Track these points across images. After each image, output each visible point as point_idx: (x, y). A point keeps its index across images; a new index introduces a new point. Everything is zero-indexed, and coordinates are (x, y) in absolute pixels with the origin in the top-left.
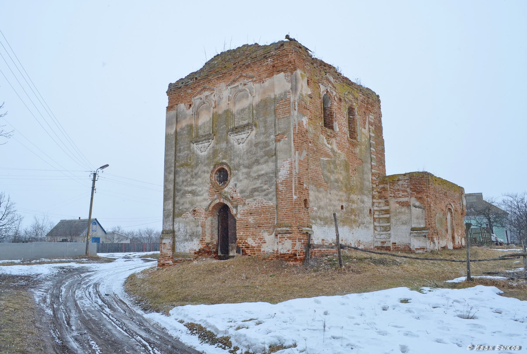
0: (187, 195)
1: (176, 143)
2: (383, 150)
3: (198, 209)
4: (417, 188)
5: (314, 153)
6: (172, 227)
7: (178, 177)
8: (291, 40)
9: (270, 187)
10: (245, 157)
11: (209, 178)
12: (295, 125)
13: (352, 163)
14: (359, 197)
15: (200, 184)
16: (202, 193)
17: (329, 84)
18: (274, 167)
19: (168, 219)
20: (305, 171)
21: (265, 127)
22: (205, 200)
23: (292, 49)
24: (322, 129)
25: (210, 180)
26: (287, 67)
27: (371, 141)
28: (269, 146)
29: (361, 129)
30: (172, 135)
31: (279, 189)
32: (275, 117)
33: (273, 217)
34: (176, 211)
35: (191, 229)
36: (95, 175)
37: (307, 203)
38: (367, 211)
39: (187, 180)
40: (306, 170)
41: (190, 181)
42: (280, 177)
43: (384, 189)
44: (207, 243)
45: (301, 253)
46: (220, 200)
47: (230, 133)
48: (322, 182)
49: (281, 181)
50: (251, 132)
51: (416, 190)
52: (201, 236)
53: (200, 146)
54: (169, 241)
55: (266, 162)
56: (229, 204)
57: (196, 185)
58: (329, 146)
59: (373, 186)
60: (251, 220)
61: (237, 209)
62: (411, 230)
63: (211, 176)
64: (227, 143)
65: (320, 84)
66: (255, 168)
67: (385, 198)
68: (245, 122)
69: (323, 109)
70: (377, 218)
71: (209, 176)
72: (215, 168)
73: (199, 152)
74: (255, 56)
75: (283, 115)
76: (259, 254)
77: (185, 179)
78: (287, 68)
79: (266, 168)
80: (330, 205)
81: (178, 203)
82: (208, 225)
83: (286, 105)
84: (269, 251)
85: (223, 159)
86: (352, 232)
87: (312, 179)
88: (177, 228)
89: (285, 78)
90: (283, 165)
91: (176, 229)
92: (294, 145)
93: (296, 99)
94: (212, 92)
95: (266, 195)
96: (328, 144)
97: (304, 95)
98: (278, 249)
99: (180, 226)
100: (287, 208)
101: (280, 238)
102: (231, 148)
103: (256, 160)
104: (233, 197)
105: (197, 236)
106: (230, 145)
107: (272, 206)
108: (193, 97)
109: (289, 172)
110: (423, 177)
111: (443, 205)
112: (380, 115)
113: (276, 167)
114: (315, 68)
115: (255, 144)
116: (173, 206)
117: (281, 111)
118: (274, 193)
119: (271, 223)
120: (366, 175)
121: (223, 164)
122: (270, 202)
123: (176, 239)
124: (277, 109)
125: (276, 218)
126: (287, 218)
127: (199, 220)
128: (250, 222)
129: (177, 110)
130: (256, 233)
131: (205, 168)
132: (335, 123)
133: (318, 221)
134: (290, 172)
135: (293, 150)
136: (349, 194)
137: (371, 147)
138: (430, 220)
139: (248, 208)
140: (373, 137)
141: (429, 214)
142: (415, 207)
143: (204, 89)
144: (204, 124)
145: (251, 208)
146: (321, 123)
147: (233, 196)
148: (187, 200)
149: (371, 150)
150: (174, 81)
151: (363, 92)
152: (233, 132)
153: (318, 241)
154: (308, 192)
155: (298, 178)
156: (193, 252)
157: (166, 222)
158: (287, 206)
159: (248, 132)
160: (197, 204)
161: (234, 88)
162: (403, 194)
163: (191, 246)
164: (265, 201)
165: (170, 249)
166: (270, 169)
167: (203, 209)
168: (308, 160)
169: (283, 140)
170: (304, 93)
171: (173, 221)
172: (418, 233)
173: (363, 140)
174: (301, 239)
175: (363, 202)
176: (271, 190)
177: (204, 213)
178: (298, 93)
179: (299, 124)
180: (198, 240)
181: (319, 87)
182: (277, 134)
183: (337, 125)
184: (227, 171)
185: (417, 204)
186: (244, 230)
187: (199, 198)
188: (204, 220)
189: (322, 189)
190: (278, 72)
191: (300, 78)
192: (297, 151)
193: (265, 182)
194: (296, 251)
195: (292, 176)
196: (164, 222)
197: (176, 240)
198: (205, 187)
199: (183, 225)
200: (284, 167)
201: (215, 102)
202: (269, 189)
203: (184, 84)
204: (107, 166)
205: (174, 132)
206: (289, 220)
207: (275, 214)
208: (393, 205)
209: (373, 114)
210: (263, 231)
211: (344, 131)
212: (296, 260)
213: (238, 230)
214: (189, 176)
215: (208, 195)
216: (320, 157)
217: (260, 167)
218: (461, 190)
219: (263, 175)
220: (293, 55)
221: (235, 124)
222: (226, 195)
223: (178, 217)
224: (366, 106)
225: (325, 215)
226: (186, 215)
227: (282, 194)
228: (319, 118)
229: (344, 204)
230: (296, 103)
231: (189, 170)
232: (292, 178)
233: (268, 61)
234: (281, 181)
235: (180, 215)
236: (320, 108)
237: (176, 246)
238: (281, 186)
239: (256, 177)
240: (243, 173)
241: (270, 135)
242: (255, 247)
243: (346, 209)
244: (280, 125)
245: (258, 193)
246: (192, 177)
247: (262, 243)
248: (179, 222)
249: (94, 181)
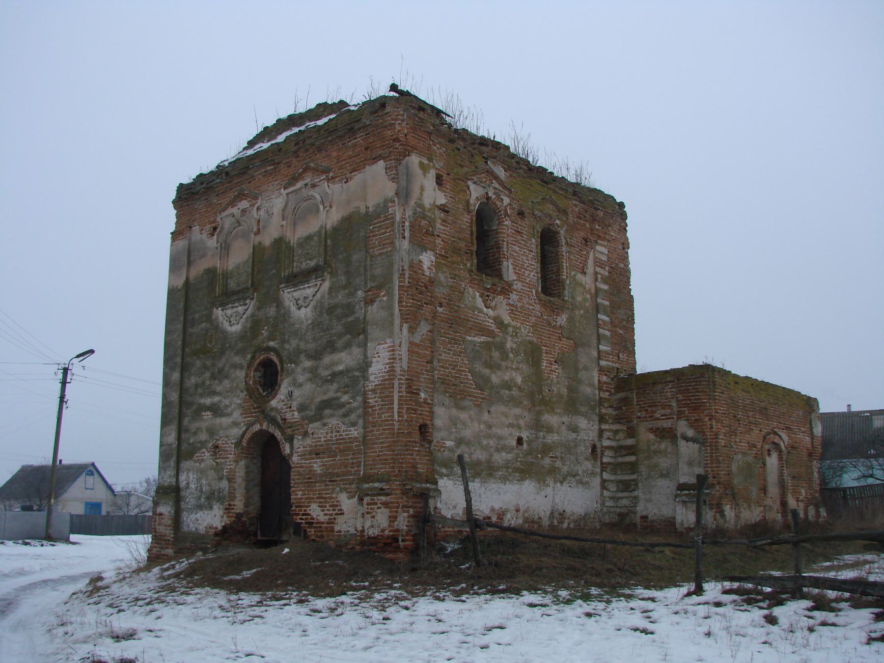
0: (204, 413)
1: (186, 308)
2: (631, 319)
3: (223, 444)
4: (690, 400)
5: (451, 327)
6: (175, 480)
8: (401, 93)
9: (353, 398)
10: (309, 336)
11: (244, 380)
12: (403, 270)
13: (548, 347)
14: (565, 419)
15: (228, 392)
16: (229, 410)
17: (494, 181)
18: (362, 357)
19: (168, 464)
20: (424, 365)
21: (347, 273)
22: (235, 424)
23: (401, 112)
24: (470, 275)
25: (244, 383)
26: (391, 149)
27: (599, 300)
28: (353, 312)
29: (575, 275)
30: (179, 290)
31: (369, 403)
32: (367, 252)
33: (357, 462)
34: (183, 448)
35: (209, 485)
36: (66, 371)
37: (427, 432)
38: (584, 450)
39: (204, 383)
40: (427, 362)
41: (210, 385)
42: (372, 378)
43: (626, 401)
44: (237, 514)
45: (407, 535)
46: (261, 425)
47: (282, 286)
48: (468, 387)
49: (373, 387)
50: (321, 284)
51: (688, 404)
52: (227, 498)
53: (229, 312)
54: (169, 509)
55: (347, 346)
56: (278, 434)
57: (219, 394)
58: (491, 312)
59: (602, 395)
60: (317, 466)
62: (678, 490)
63: (247, 376)
64: (277, 307)
65: (469, 183)
66: (327, 359)
67: (628, 422)
68: (312, 264)
69: (475, 234)
70: (609, 464)
71: (244, 375)
72: (253, 358)
73: (226, 325)
74: (335, 128)
75: (380, 249)
76: (331, 538)
77: (200, 380)
78: (391, 152)
79: (345, 359)
80: (490, 437)
81: (187, 430)
82: (239, 477)
83: (387, 228)
84: (348, 531)
85: (269, 339)
86: (543, 493)
87: (442, 383)
88: (184, 483)
89: (386, 173)
90: (378, 353)
91: (183, 484)
92: (400, 310)
93: (407, 216)
94: (254, 202)
95: (345, 415)
96: (487, 307)
97: (427, 206)
98: (363, 527)
99: (189, 478)
100: (381, 443)
101: (368, 504)
102: (284, 316)
103: (330, 341)
104: (285, 419)
105: (220, 500)
106: (282, 310)
107: (355, 438)
108: (220, 213)
109: (388, 366)
110: (702, 375)
111: (755, 436)
112: (626, 245)
113: (365, 356)
114: (459, 150)
115: (329, 309)
116: (177, 436)
117: (376, 240)
118: (360, 410)
119: (353, 472)
120: (584, 372)
121: (269, 349)
122: (352, 429)
123: (183, 505)
124: (371, 236)
125: (362, 463)
126: (381, 464)
127: (223, 466)
128: (315, 470)
130: (325, 494)
131: (237, 359)
132: (505, 263)
133: (455, 469)
134: (389, 367)
135: (397, 321)
136: (540, 413)
137: (598, 312)
138: (717, 467)
139: (313, 442)
140: (605, 291)
141: (714, 455)
142: (687, 439)
143: (241, 196)
144: (238, 267)
145: (318, 441)
146: (468, 265)
147: (287, 417)
148: (204, 425)
149: (598, 319)
150: (186, 181)
151: (580, 198)
152: (288, 285)
153: (453, 511)
154: (431, 408)
155: (406, 379)
156: (212, 532)
157: (165, 470)
158: (383, 438)
159: (316, 285)
160: (221, 433)
161: (294, 194)
162: (663, 412)
163: (210, 520)
164: (343, 428)
165: (169, 526)
166: (354, 360)
167: (232, 443)
168: (433, 342)
169: (380, 301)
170: (427, 202)
172: (690, 494)
173: (579, 298)
174: (409, 507)
175: (575, 429)
176: (355, 404)
177: (233, 452)
178: (412, 203)
179: (411, 266)
180: (221, 507)
181: (468, 188)
182: (369, 286)
183: (511, 267)
184: (276, 364)
185: (690, 433)
186: (305, 487)
187: (225, 421)
188: (233, 467)
189: (467, 403)
190: (374, 159)
191: (419, 171)
192: (406, 323)
194: (398, 530)
195: (393, 375)
196: (162, 469)
198: (235, 399)
199: (195, 476)
200: (379, 357)
201: (259, 221)
202: (351, 403)
203: (204, 185)
204: (92, 352)
205: (184, 284)
206: (386, 468)
207: (360, 454)
208: (645, 436)
209: (605, 243)
210: (338, 489)
211: (528, 280)
212: (398, 549)
213: (294, 487)
214: (207, 375)
215: (242, 414)
216: (465, 334)
217: (336, 357)
218: (810, 404)
219: (341, 373)
220: (404, 124)
221: (293, 267)
222: (273, 414)
223: (186, 460)
224: (588, 225)
225: (474, 457)
226: (201, 456)
227: (375, 414)
228: (466, 253)
229: (524, 435)
230: (407, 224)
231: (209, 363)
232: (394, 379)
233: (357, 138)
234: (373, 387)
235: (190, 455)
236: (469, 233)
238: (373, 396)
239: (329, 377)
240: (304, 369)
241: (356, 290)
242: (323, 523)
243: (529, 444)
244: (373, 270)
245: (332, 411)
246: (213, 377)
247: (336, 514)
248: (189, 470)
249: (64, 383)
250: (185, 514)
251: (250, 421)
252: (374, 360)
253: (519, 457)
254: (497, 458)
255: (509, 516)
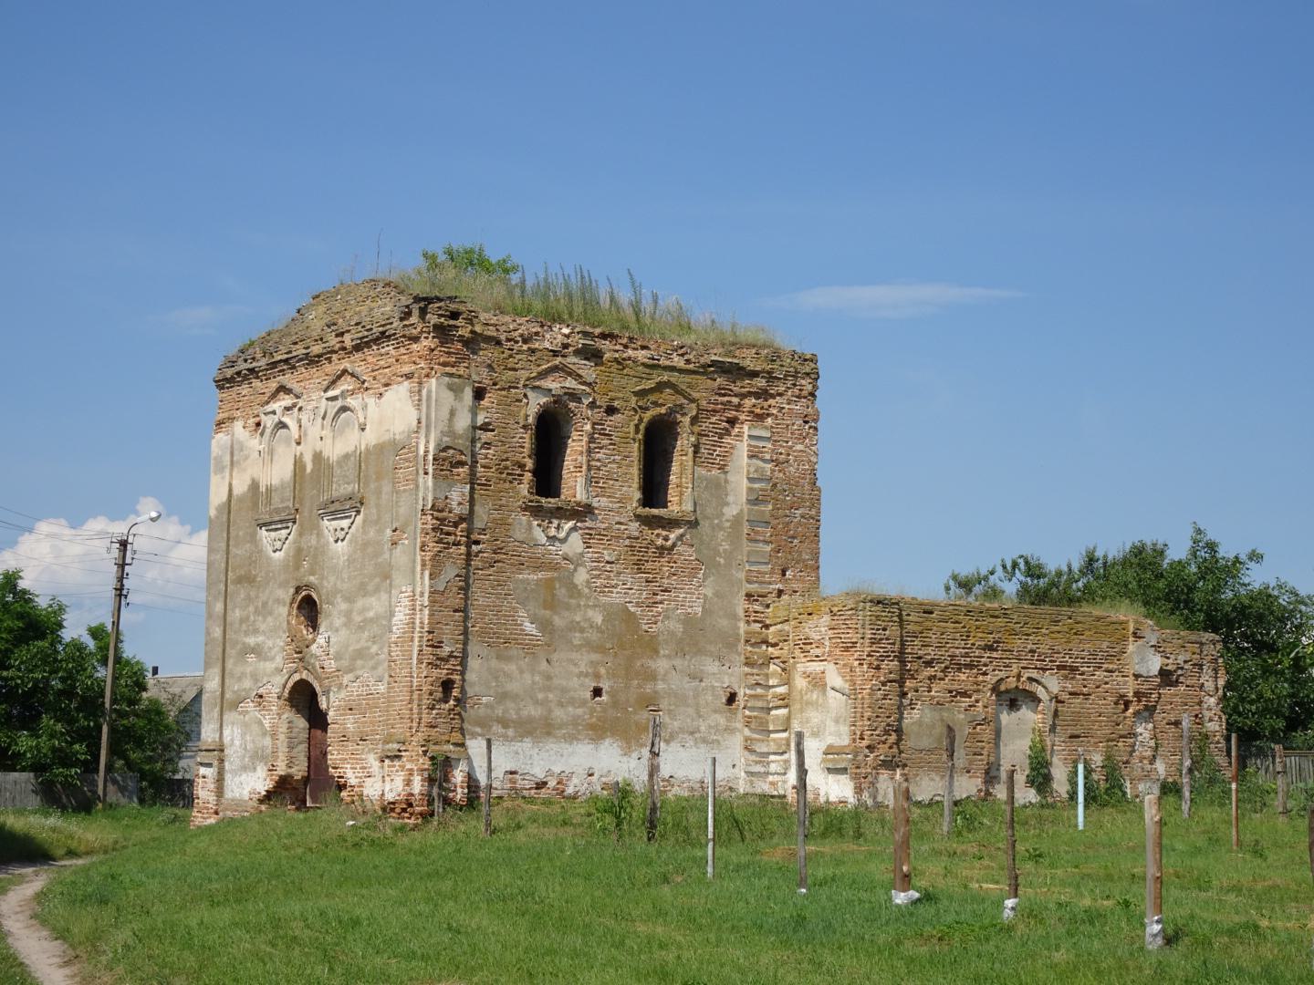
7: (233, 611)
16: (273, 653)
36: (124, 544)
55: (377, 590)
61: (328, 699)
66: (360, 603)
80: (548, 689)
88: (229, 738)
91: (227, 740)
105: (263, 758)
123: (227, 765)
129: (233, 435)
148: (249, 669)
165: (212, 791)
171: (222, 719)
187: (269, 666)
189: (514, 652)
193: (374, 637)
197: (227, 768)
214: (251, 609)
219: (371, 620)
235: (235, 705)
237: (226, 784)
247: (365, 777)
248: (233, 724)
250: (228, 777)
251: (291, 667)
252: (397, 609)
253: (595, 711)
254: (558, 713)
255: (575, 781)
